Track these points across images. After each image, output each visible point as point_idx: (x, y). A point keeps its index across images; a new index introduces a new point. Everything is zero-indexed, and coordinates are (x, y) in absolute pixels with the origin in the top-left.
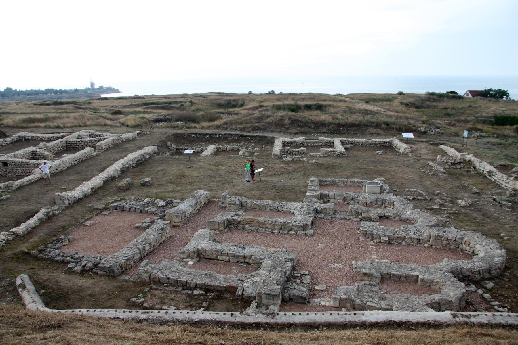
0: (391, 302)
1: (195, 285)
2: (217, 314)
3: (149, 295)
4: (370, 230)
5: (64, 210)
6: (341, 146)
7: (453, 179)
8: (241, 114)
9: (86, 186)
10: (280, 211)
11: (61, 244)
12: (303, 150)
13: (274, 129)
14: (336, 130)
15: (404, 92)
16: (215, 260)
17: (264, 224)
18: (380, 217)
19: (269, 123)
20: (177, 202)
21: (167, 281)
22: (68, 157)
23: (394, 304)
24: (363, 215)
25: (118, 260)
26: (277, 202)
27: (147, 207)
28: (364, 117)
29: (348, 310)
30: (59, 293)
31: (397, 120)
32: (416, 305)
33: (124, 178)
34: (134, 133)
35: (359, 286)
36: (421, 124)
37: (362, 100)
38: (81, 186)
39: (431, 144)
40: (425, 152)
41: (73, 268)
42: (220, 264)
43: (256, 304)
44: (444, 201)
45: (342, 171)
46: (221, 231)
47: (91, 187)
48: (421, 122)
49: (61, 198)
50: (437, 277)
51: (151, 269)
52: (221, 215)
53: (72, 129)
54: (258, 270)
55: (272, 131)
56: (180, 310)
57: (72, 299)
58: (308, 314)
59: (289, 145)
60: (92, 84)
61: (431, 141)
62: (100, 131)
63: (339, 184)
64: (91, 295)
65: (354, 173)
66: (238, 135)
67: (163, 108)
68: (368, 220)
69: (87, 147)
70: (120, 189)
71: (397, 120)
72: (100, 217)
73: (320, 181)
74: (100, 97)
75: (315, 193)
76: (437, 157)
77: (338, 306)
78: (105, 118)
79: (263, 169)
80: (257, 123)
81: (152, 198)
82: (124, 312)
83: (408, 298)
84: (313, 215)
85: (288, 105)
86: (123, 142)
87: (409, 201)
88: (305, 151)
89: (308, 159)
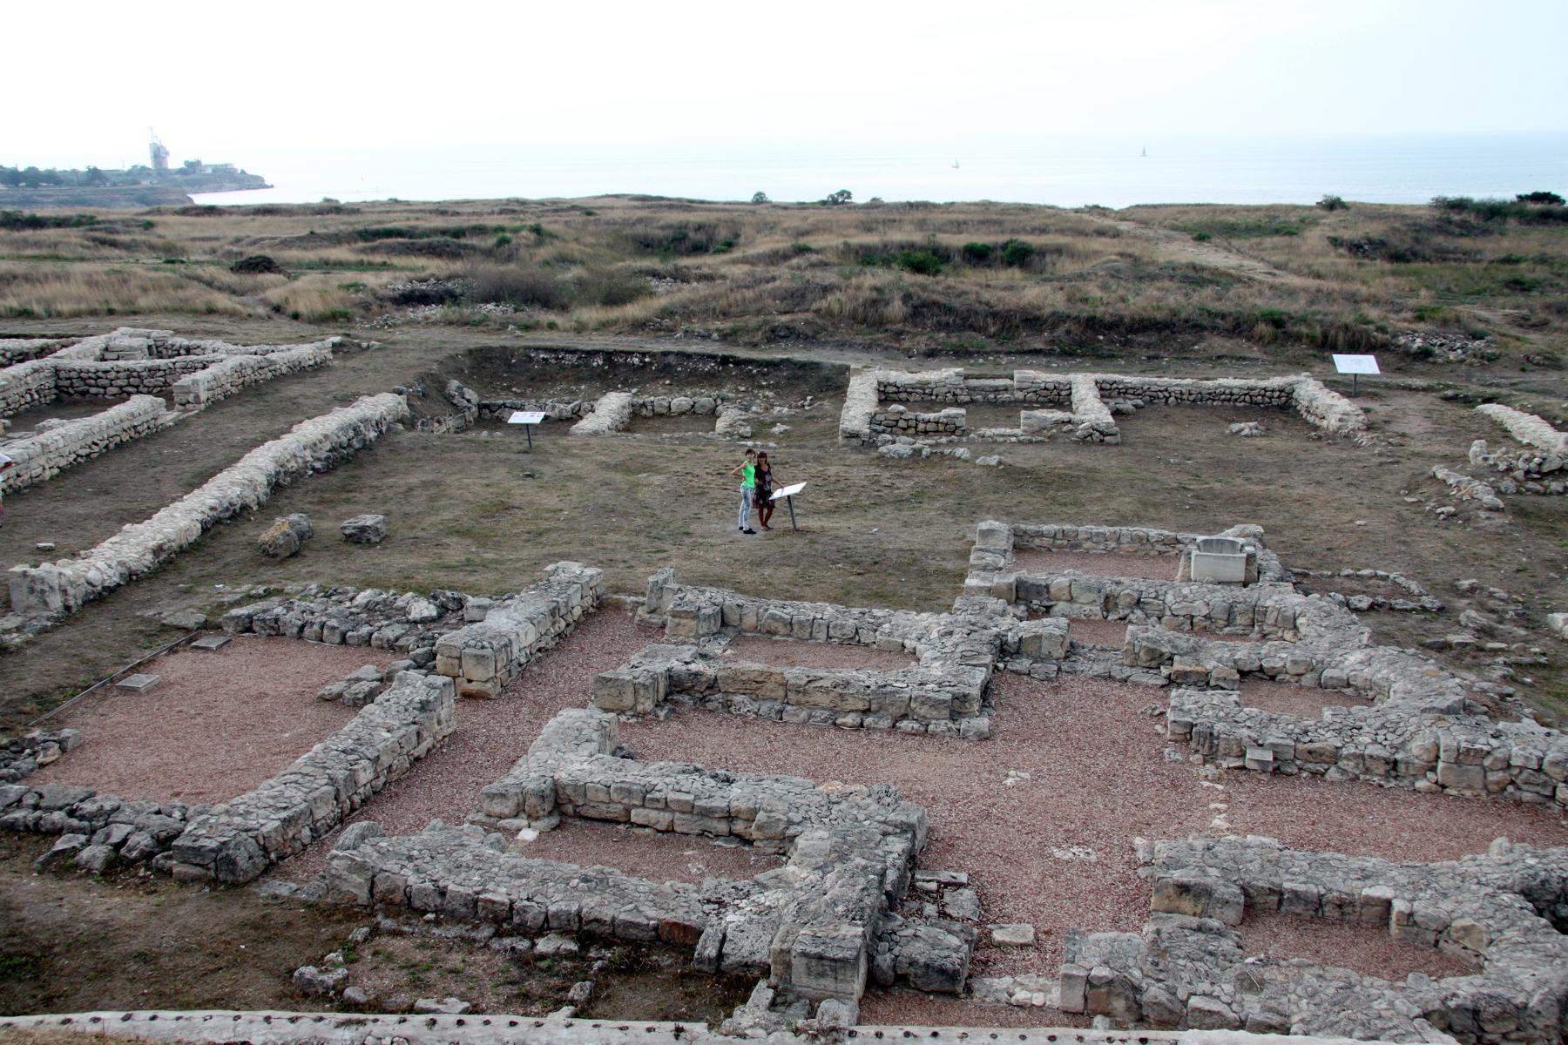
0: (1284, 1000)
1: (542, 917)
2: (621, 1029)
3: (367, 954)
4: (1204, 720)
5: (44, 630)
6: (1097, 404)
7: (1534, 532)
8: (723, 277)
9: (132, 540)
10: (867, 645)
11: (30, 759)
12: (956, 417)
13: (847, 337)
14: (1081, 344)
15: (1344, 199)
16: (619, 823)
17: (805, 693)
18: (1243, 674)
19: (829, 313)
20: (478, 607)
21: (438, 901)
22: (62, 430)
23: (1294, 1008)
24: (1178, 666)
25: (252, 823)
26: (856, 611)
27: (367, 623)
28: (1186, 295)
29: (1119, 1026)
30: (12, 950)
31: (1314, 308)
32: (1384, 1013)
33: (281, 513)
34: (319, 344)
35: (1158, 932)
36: (1410, 322)
37: (1184, 229)
38: (113, 539)
39: (1447, 399)
40: (1421, 430)
41: (75, 851)
42: (638, 837)
43: (770, 993)
44: (1494, 617)
45: (1099, 499)
46: (645, 714)
47: (152, 544)
48: (1409, 315)
49: (35, 587)
50: (1467, 908)
51: (375, 855)
52: (645, 656)
53: (80, 322)
54: (778, 864)
55: (841, 346)
56: (482, 1012)
57: (67, 971)
58: (965, 1035)
59: (903, 396)
60: (159, 154)
61: (1448, 387)
62: (191, 333)
63: (1087, 545)
64: (142, 957)
65: (1145, 504)
66: (713, 357)
67: (433, 251)
68: (1195, 683)
69: (139, 392)
70: (266, 553)
71: (1314, 308)
72: (186, 658)
73: (1017, 534)
74: (188, 205)
75: (996, 580)
76: (1469, 446)
77: (1080, 1008)
78: (210, 284)
79: (803, 485)
80: (786, 313)
81: (387, 589)
82: (268, 1019)
83: (1350, 986)
84: (988, 659)
85: (902, 247)
86: (279, 378)
87: (1354, 616)
88: (962, 422)
89: (972, 452)
